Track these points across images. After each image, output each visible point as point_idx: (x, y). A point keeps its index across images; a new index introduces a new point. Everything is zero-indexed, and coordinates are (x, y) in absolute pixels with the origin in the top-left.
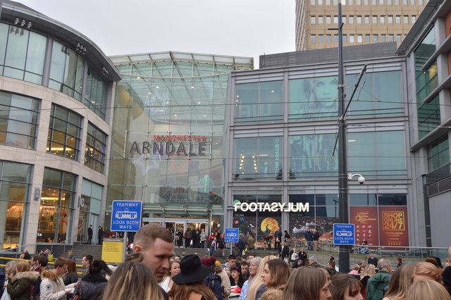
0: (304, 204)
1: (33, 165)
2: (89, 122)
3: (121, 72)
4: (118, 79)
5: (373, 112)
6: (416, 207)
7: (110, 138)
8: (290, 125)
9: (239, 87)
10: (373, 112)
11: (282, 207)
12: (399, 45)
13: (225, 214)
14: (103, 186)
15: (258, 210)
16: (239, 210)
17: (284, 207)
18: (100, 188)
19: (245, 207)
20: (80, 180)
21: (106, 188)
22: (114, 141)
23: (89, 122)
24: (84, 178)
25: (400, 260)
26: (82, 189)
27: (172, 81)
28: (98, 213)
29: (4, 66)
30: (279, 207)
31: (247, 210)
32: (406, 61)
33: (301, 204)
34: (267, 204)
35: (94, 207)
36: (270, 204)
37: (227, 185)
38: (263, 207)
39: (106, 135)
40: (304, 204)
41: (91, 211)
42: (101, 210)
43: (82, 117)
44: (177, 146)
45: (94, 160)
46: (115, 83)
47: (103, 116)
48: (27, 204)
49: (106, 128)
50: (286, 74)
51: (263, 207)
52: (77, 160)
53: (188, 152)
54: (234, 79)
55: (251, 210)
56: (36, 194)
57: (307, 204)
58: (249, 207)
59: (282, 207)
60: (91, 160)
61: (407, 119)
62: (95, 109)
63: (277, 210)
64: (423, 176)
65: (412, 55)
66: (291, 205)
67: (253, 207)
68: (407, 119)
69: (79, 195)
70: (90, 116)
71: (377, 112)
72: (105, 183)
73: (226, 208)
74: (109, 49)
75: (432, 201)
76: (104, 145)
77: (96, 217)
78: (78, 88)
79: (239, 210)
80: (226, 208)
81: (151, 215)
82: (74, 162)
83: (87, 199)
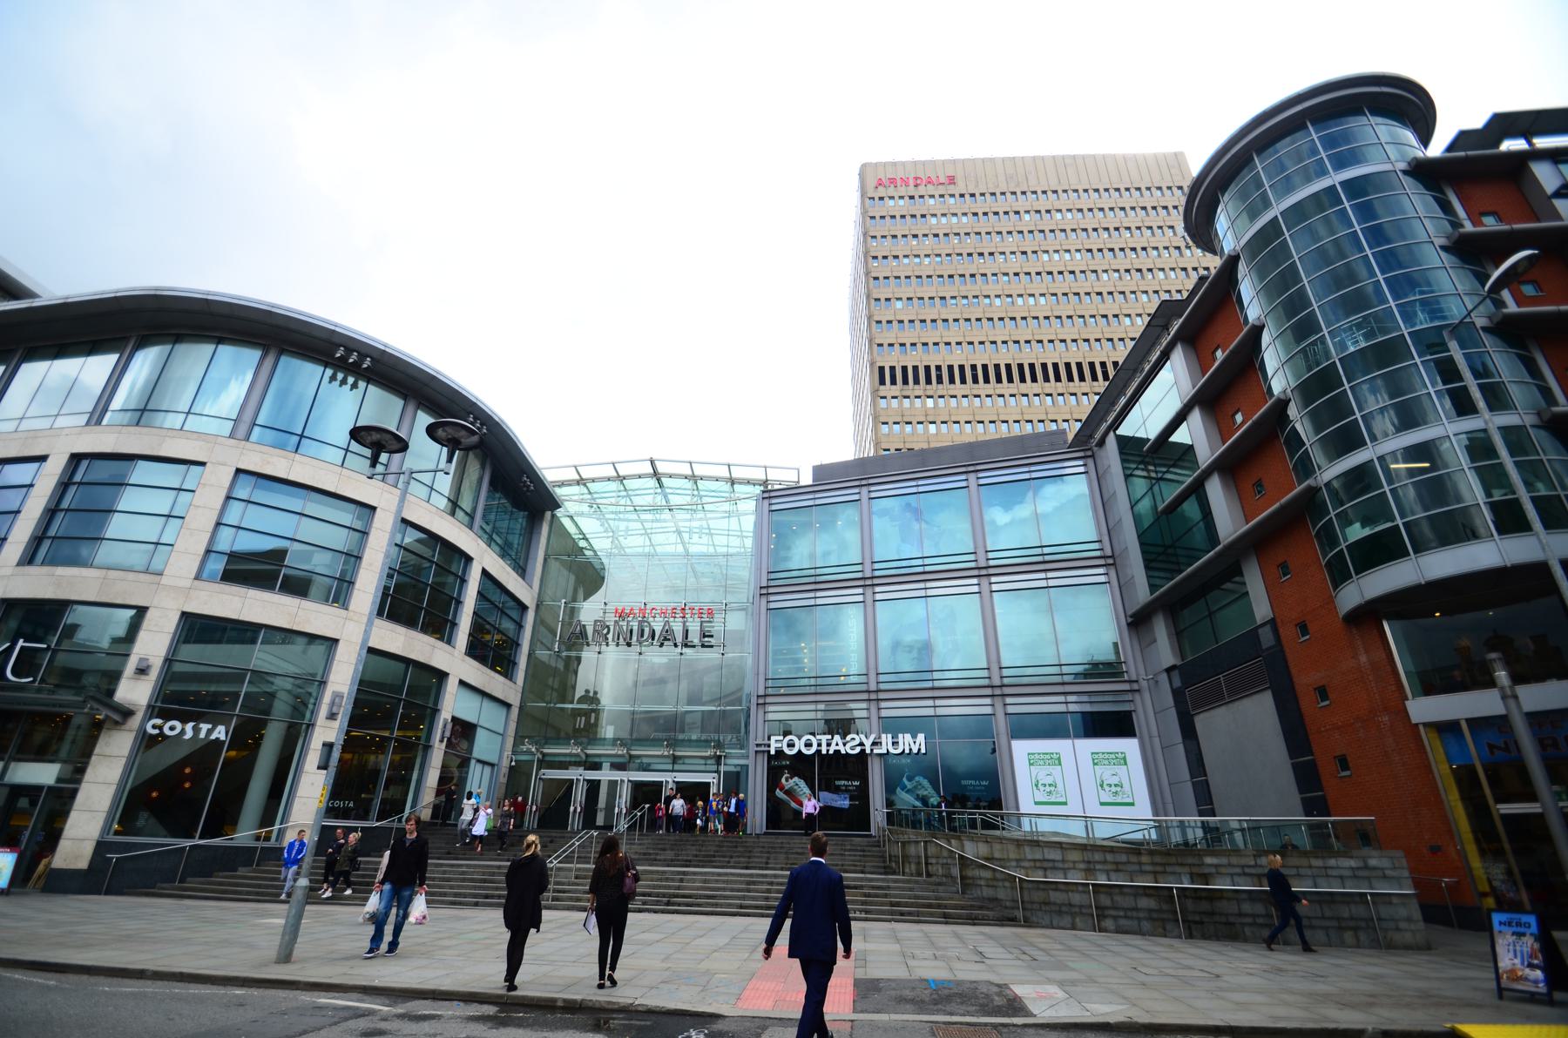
0: (914, 737)
1: (337, 641)
2: (485, 572)
3: (559, 492)
4: (554, 504)
5: (1039, 551)
6: (1157, 741)
7: (530, 617)
8: (876, 581)
9: (776, 517)
10: (1039, 551)
11: (868, 744)
12: (1070, 437)
13: (750, 762)
14: (508, 706)
15: (819, 752)
16: (779, 752)
17: (874, 744)
18: (503, 711)
19: (791, 745)
20: (451, 685)
21: (515, 711)
22: (539, 622)
23: (485, 572)
24: (462, 683)
25: (512, 987)
26: (454, 704)
27: (654, 509)
28: (493, 759)
29: (302, 436)
30: (861, 744)
31: (795, 751)
32: (1093, 456)
33: (908, 737)
34: (837, 738)
35: (483, 746)
36: (844, 737)
37: (754, 700)
38: (829, 745)
39: (523, 608)
40: (914, 737)
41: (477, 753)
42: (500, 757)
43: (469, 559)
44: (658, 629)
45: (492, 649)
46: (548, 514)
47: (522, 570)
48: (169, 661)
49: (525, 592)
50: (865, 490)
51: (829, 745)
52: (449, 642)
53: (679, 640)
54: (764, 600)
55: (805, 751)
56: (333, 704)
57: (921, 737)
58: (800, 745)
59: (868, 744)
60: (478, 650)
61: (1110, 561)
62: (504, 553)
63: (858, 750)
64: (1169, 670)
65: (1178, 355)
66: (886, 739)
67: (809, 745)
68: (1110, 561)
69: (445, 714)
70: (485, 558)
71: (1046, 550)
72: (514, 698)
73: (752, 748)
74: (547, 454)
75: (1201, 722)
76: (520, 626)
77: (487, 770)
78: (466, 503)
79: (779, 752)
80: (752, 748)
81: (606, 765)
82: (439, 644)
83: (464, 730)
